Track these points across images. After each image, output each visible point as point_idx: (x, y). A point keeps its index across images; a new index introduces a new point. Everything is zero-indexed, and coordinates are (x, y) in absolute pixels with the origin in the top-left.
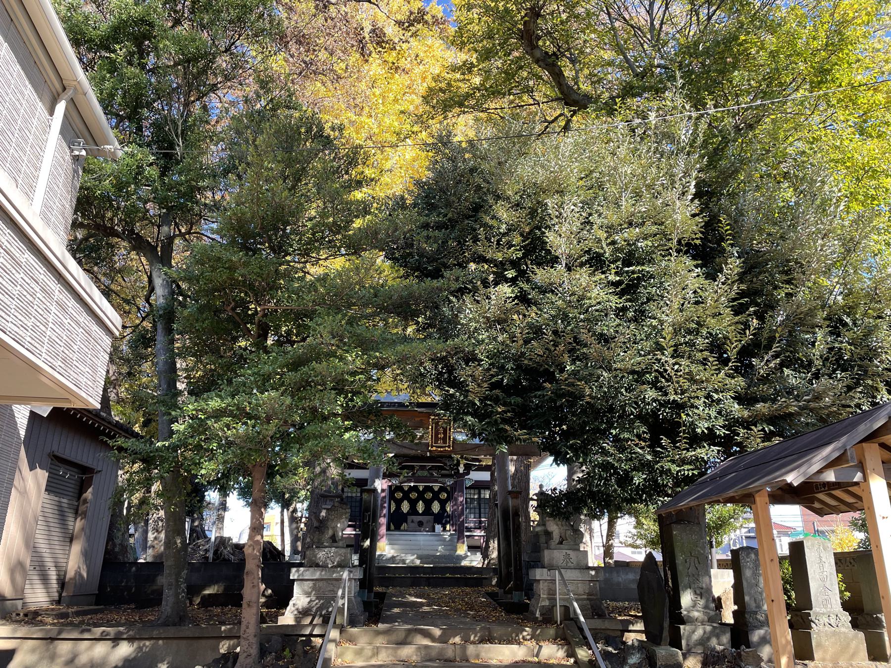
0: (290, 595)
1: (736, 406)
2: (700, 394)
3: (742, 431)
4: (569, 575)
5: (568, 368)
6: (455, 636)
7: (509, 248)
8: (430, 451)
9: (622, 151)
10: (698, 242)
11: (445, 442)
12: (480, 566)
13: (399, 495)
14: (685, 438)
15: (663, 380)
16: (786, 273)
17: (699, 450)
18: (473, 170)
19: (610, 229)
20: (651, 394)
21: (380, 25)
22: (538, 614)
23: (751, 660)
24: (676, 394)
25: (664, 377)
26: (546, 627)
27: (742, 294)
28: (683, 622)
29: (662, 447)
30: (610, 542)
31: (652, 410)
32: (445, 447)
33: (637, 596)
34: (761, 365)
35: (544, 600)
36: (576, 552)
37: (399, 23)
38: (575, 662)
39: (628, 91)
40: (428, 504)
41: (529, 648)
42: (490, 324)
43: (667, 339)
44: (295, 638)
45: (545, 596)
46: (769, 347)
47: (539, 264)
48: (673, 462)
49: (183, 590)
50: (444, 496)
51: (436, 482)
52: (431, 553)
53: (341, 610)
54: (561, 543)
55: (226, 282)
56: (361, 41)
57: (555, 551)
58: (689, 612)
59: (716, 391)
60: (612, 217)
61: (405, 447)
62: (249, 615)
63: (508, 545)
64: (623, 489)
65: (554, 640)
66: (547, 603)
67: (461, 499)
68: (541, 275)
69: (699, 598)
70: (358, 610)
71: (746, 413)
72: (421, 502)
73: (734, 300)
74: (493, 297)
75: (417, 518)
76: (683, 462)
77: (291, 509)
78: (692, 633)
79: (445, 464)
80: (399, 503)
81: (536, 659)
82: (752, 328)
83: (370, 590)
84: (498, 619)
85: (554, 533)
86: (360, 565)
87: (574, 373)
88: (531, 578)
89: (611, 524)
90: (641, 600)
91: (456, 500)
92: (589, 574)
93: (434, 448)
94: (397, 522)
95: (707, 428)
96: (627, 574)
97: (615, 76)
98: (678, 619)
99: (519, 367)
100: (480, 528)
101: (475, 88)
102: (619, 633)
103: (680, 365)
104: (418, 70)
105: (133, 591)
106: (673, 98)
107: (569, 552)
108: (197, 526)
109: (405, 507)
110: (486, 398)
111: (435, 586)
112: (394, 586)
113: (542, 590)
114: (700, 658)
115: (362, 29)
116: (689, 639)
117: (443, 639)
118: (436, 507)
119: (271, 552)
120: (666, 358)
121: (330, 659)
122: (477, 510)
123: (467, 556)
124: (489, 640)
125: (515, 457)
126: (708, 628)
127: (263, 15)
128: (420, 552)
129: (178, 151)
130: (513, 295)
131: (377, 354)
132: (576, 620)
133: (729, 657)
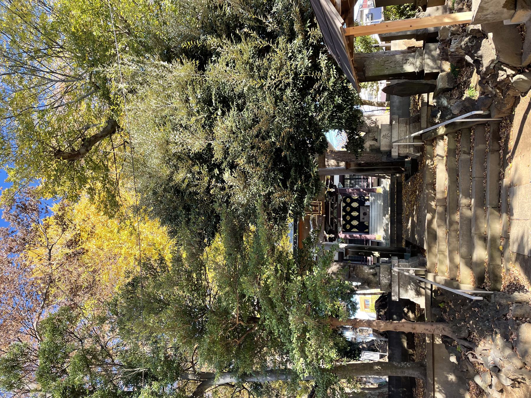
0: (408, 300)
1: (295, 42)
2: (288, 63)
3: (311, 40)
5: (273, 140)
6: (432, 205)
7: (201, 173)
8: (323, 215)
9: (142, 106)
10: (198, 62)
11: (317, 206)
12: (389, 180)
13: (348, 227)
14: (315, 74)
15: (280, 85)
16: (216, 7)
17: (322, 65)
18: (155, 193)
19: (190, 114)
20: (288, 92)
21: (65, 242)
22: (418, 154)
23: (445, 34)
24: (289, 78)
25: (279, 85)
27: (228, 36)
28: (423, 71)
29: (320, 86)
31: (298, 92)
33: (408, 97)
34: (271, 25)
35: (410, 151)
36: (382, 131)
37: (64, 230)
38: (446, 135)
39: (106, 95)
40: (353, 209)
42: (246, 185)
43: (255, 83)
44: (433, 299)
46: (261, 22)
47: (212, 156)
48: (329, 80)
49: (405, 364)
50: (348, 200)
51: (340, 205)
52: (382, 208)
53: (416, 272)
54: (376, 140)
55: (223, 345)
56: (75, 255)
58: (417, 67)
59: (287, 53)
60: (183, 113)
62: (420, 328)
63: (378, 169)
64: (344, 109)
65: (434, 147)
66: (412, 149)
67: (350, 190)
68: (218, 155)
69: (408, 61)
70: (416, 260)
71: (300, 37)
73: (232, 41)
74: (231, 184)
75: (362, 216)
76: (328, 74)
77: (356, 289)
78: (429, 67)
80: (352, 227)
81: (445, 158)
82: (250, 32)
83: (404, 251)
84: (421, 178)
85: (371, 144)
86: (390, 257)
87: (276, 136)
88: (397, 157)
89: (364, 103)
90: (410, 95)
91: (350, 193)
93: (321, 212)
94: (364, 228)
95: (309, 60)
97: (96, 102)
98: (420, 74)
99: (273, 169)
100: (367, 179)
101: (104, 187)
103: (272, 75)
104: (93, 219)
106: (111, 72)
107: (382, 136)
108: (367, 345)
110: (292, 189)
111: (402, 210)
112: (402, 234)
113: (404, 152)
114: (444, 62)
115: (67, 254)
116: (432, 68)
117: (433, 211)
118: (355, 205)
119: (381, 301)
120: (268, 83)
121: (445, 280)
122: (357, 180)
123: (384, 187)
125: (326, 160)
126: (426, 56)
127: (59, 319)
128: (382, 214)
129: (142, 370)
130: (229, 171)
131: (265, 256)
132: (421, 134)
133: (444, 46)
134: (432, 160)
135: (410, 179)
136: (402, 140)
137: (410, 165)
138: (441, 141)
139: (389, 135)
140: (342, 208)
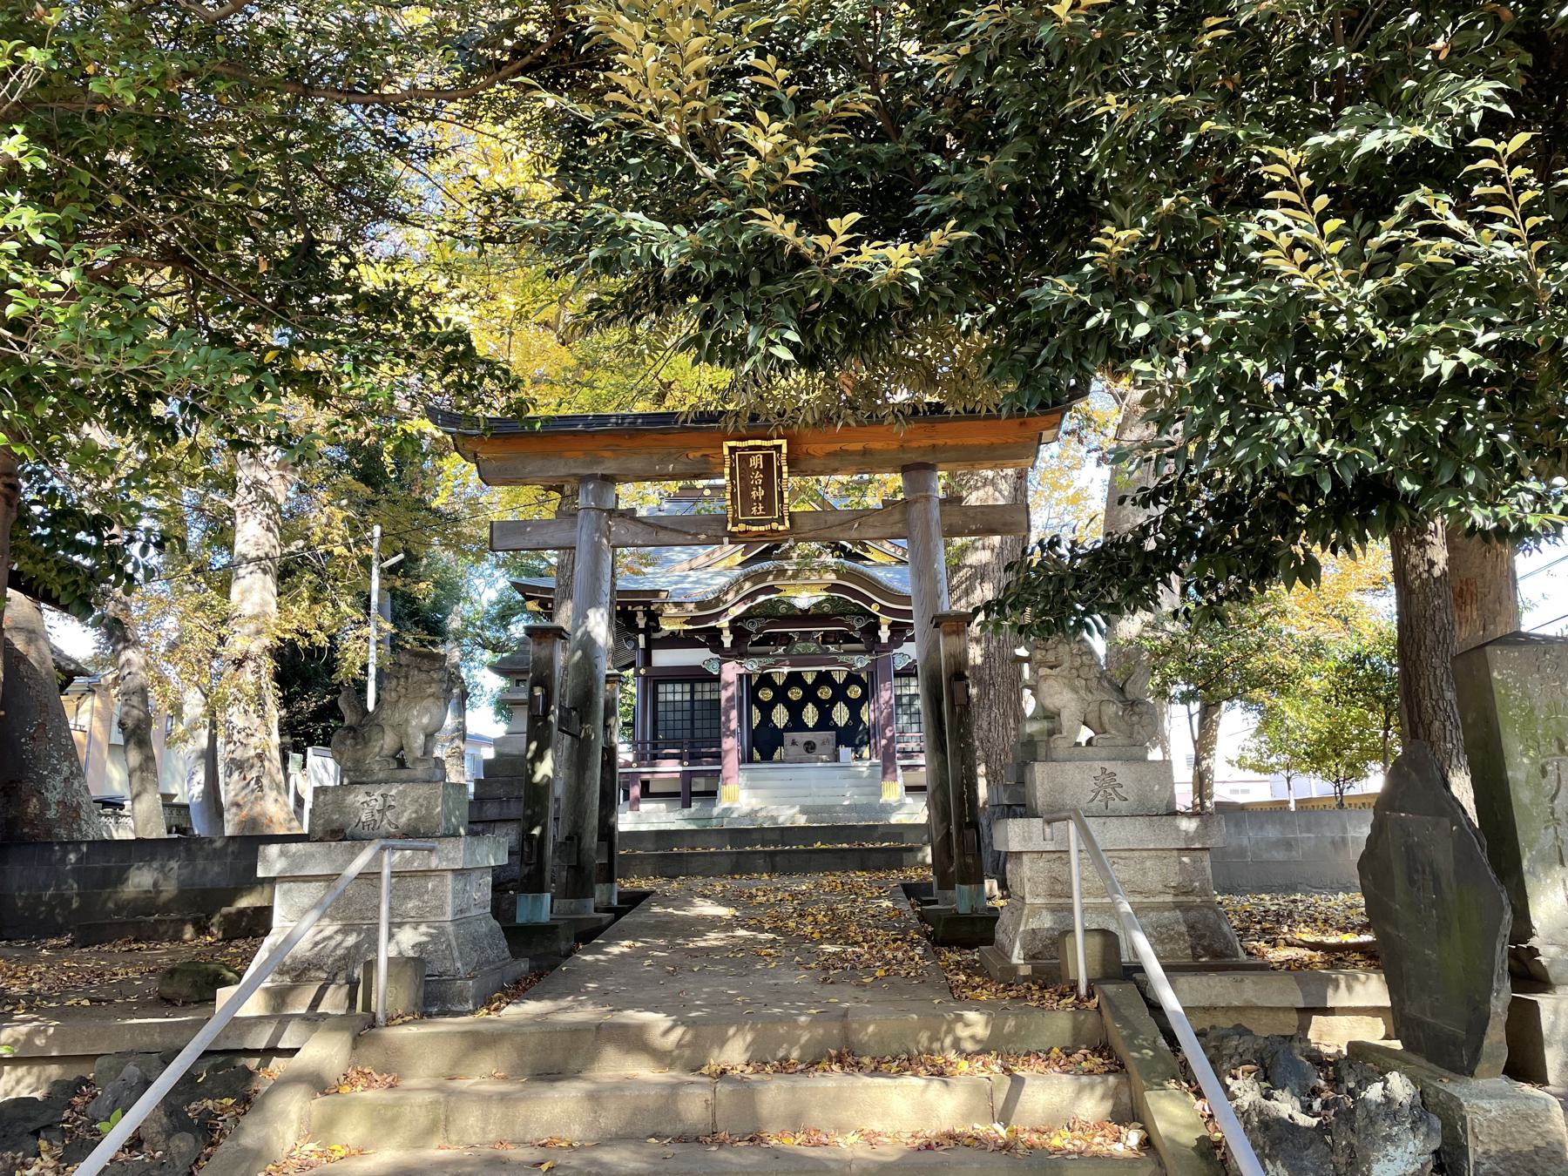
4: (1110, 834)
13: (766, 695)
22: (1017, 957)
26: (1041, 1007)
30: (1204, 764)
32: (773, 520)
35: (1035, 911)
36: (1135, 767)
38: (1147, 1143)
40: (825, 710)
41: (976, 1088)
45: (1039, 901)
50: (855, 692)
51: (834, 662)
57: (1069, 766)
61: (665, 528)
63: (943, 765)
65: (1065, 1057)
66: (1046, 921)
72: (810, 706)
79: (852, 628)
80: (767, 709)
92: (1177, 829)
93: (742, 527)
94: (763, 745)
96: (1261, 827)
102: (1290, 1023)
105: (75, 905)
109: (780, 716)
111: (788, 871)
113: (1029, 877)
118: (841, 714)
123: (901, 805)
124: (840, 1060)
128: (809, 801)
134: (985, 1049)
135: (905, 906)
136: (1101, 867)
137: (963, 908)
138: (1108, 1106)
139: (1116, 803)
140: (823, 669)
